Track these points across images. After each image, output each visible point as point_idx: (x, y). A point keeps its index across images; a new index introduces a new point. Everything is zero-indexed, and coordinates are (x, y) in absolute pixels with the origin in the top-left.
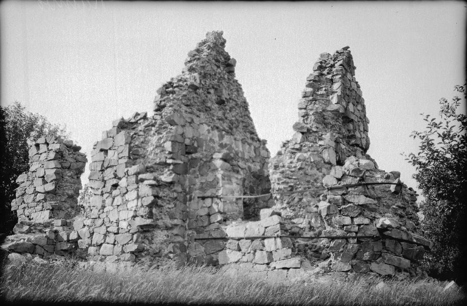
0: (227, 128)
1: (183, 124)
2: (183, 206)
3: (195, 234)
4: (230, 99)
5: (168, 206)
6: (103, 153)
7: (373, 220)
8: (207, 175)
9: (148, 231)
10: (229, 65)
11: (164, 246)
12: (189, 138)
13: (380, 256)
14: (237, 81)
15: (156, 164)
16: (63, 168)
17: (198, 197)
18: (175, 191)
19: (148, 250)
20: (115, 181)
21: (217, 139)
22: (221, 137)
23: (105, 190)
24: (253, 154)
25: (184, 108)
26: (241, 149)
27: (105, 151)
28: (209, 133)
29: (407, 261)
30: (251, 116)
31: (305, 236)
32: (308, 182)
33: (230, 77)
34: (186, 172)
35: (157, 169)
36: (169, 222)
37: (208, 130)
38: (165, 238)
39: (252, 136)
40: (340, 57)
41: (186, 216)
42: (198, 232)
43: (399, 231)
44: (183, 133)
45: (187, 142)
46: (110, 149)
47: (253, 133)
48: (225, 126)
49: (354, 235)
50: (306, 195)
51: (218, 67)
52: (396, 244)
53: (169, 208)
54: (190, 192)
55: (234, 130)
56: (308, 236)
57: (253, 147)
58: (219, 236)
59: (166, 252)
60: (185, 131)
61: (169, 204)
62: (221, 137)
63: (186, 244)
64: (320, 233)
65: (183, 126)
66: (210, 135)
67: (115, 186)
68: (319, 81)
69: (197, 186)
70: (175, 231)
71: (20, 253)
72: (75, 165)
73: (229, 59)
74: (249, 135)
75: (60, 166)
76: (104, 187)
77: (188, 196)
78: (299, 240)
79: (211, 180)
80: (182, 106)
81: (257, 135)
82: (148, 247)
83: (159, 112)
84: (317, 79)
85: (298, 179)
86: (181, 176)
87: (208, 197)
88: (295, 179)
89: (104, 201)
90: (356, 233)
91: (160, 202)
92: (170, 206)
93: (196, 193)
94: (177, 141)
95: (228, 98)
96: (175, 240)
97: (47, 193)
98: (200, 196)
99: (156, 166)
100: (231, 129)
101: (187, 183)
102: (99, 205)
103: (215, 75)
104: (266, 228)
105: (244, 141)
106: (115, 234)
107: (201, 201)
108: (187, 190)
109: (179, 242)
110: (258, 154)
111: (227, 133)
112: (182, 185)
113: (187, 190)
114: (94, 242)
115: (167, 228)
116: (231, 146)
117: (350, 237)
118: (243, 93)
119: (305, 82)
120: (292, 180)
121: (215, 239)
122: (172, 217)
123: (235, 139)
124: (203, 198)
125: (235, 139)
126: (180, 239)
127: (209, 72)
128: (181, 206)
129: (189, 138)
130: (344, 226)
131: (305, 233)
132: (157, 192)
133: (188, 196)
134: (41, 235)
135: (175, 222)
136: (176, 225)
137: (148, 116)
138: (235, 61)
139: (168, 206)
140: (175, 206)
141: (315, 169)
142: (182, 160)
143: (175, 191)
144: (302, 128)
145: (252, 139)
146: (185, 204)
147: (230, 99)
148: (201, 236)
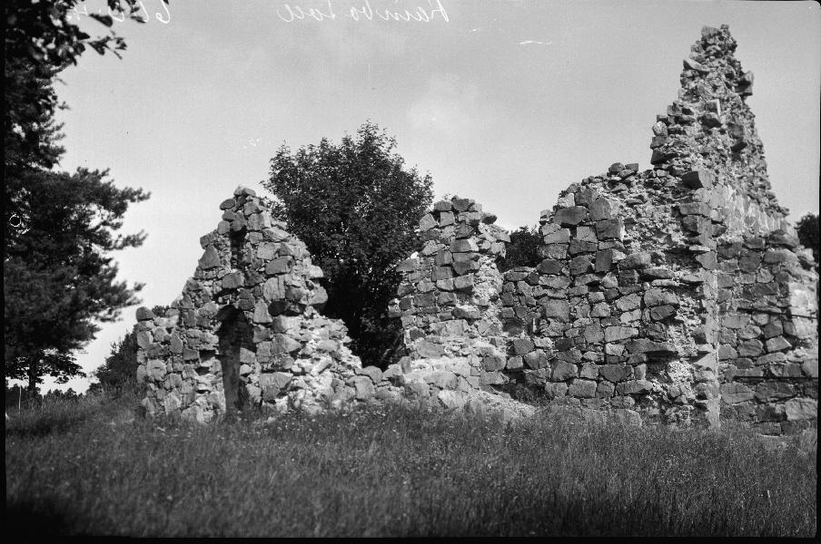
20: (591, 278)
42: (742, 366)
46: (581, 224)
61: (692, 318)
67: (594, 286)
76: (572, 285)
87: (761, 312)
92: (694, 322)
148: (752, 371)
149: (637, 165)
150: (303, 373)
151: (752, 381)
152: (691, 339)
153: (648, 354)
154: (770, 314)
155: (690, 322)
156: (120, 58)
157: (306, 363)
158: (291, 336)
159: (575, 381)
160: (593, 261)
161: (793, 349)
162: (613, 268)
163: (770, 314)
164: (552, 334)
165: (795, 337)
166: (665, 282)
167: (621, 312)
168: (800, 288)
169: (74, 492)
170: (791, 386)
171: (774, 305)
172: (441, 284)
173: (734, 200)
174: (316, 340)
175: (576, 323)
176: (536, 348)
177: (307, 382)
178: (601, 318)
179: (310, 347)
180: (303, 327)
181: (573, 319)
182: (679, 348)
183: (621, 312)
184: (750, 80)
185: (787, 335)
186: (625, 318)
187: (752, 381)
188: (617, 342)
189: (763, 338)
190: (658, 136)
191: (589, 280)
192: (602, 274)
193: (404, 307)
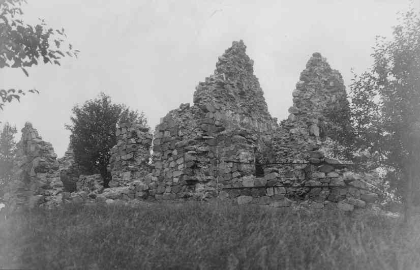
0: (246, 112)
1: (213, 111)
2: (214, 167)
3: (222, 185)
4: (249, 90)
5: (205, 168)
6: (161, 133)
7: (341, 175)
8: (230, 146)
9: (191, 184)
10: (249, 66)
11: (202, 193)
12: (218, 121)
13: (344, 198)
14: (255, 76)
15: (195, 139)
16: (137, 143)
17: (225, 161)
18: (209, 157)
19: (192, 196)
20: (169, 152)
21: (238, 120)
22: (242, 118)
23: (163, 158)
24: (266, 129)
25: (214, 99)
26: (257, 126)
27: (163, 132)
28: (233, 116)
29: (363, 202)
30: (266, 101)
31: (294, 186)
32: (298, 149)
33: (249, 74)
34: (216, 144)
35: (197, 143)
36: (205, 178)
37: (232, 114)
38: (203, 189)
39: (266, 116)
40: (339, 77)
41: (217, 173)
42: (225, 184)
43: (359, 182)
44: (214, 117)
45: (217, 123)
46: (166, 130)
47: (267, 114)
48: (245, 110)
49: (327, 184)
50: (296, 158)
51: (241, 67)
52: (356, 191)
53: (205, 169)
54: (219, 159)
55: (252, 112)
56: (297, 186)
57: (266, 124)
58: (238, 187)
59: (204, 197)
60: (215, 116)
61: (205, 166)
62: (242, 118)
63: (217, 192)
64: (304, 184)
65: (214, 113)
66: (234, 117)
67: (170, 155)
68: (310, 75)
69: (224, 154)
70: (209, 184)
71: (113, 199)
72: (145, 141)
73: (249, 60)
74: (263, 116)
75: (135, 142)
76: (163, 155)
77: (218, 161)
78: (290, 188)
79: (232, 149)
80: (214, 98)
81: (270, 115)
82: (192, 194)
83: (197, 104)
84: (308, 74)
85: (291, 147)
86: (213, 148)
87: (231, 162)
88: (289, 147)
89: (163, 165)
90: (329, 183)
91: (199, 165)
92: (205, 168)
93: (223, 159)
94: (209, 124)
95: (247, 89)
96: (210, 190)
97: (128, 160)
98: (226, 160)
99: (195, 141)
100: (250, 112)
101: (217, 152)
102: (160, 167)
103: (238, 73)
104: (268, 180)
105: (259, 120)
106: (171, 186)
107: (226, 164)
108: (217, 156)
109: (212, 191)
110: (270, 128)
111: (246, 115)
112: (214, 153)
113: (217, 156)
114: (159, 192)
115: (204, 182)
116: (249, 124)
117: (324, 186)
118: (259, 85)
119: (299, 76)
120: (286, 148)
121: (236, 188)
122: (207, 174)
123: (252, 119)
124: (228, 162)
125: (252, 119)
126: (213, 189)
127: (233, 72)
128: (213, 168)
129: (218, 121)
130: (320, 179)
131: (294, 184)
132: (197, 158)
133: (218, 161)
134: (126, 187)
135: (209, 177)
136: (210, 180)
137: (191, 106)
138: (253, 62)
139: (205, 168)
140: (209, 168)
141: (303, 140)
142: (213, 136)
143: (209, 157)
144: (295, 110)
145: (266, 118)
146: (216, 166)
147: (249, 90)
148: (228, 186)
149: (189, 104)
150: (49, 195)
151: (228, 190)
152: (204, 174)
153: (187, 181)
154: (233, 162)
155: (204, 167)
156: (27, 75)
157: (51, 191)
158: (42, 181)
159: (164, 193)
160: (170, 145)
161: (242, 176)
162: (176, 147)
163: (233, 162)
164: (157, 175)
165: (242, 171)
166: (191, 152)
167: (178, 165)
168: (244, 151)
169: (84, 231)
170: (239, 191)
171: (235, 159)
172: (123, 157)
173: (233, 116)
174: (55, 182)
175: (164, 171)
176: (152, 181)
177: (51, 198)
178: (172, 168)
179: (52, 184)
180: (47, 177)
181: (164, 169)
182: (198, 178)
183: (178, 165)
184: (251, 63)
185: (239, 171)
186: (179, 167)
187: (228, 190)
188: (177, 177)
189: (231, 173)
190: (198, 91)
191: (168, 153)
192: (173, 150)
193: (112, 167)
